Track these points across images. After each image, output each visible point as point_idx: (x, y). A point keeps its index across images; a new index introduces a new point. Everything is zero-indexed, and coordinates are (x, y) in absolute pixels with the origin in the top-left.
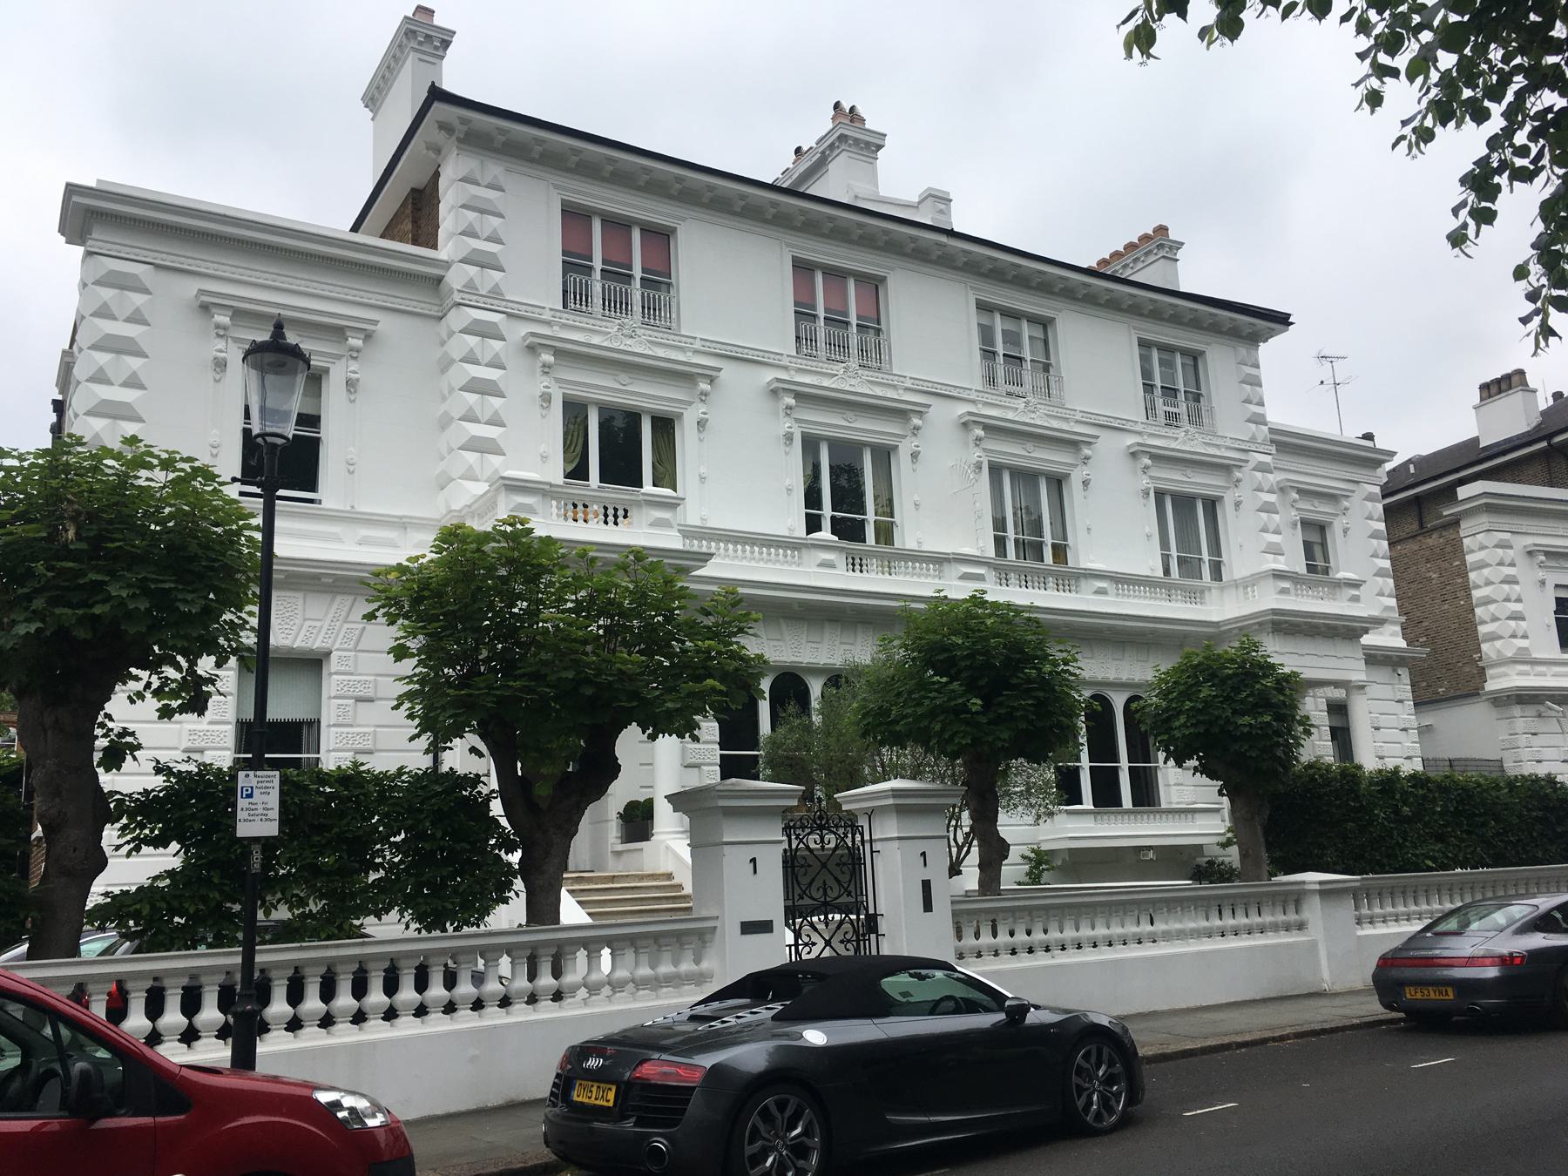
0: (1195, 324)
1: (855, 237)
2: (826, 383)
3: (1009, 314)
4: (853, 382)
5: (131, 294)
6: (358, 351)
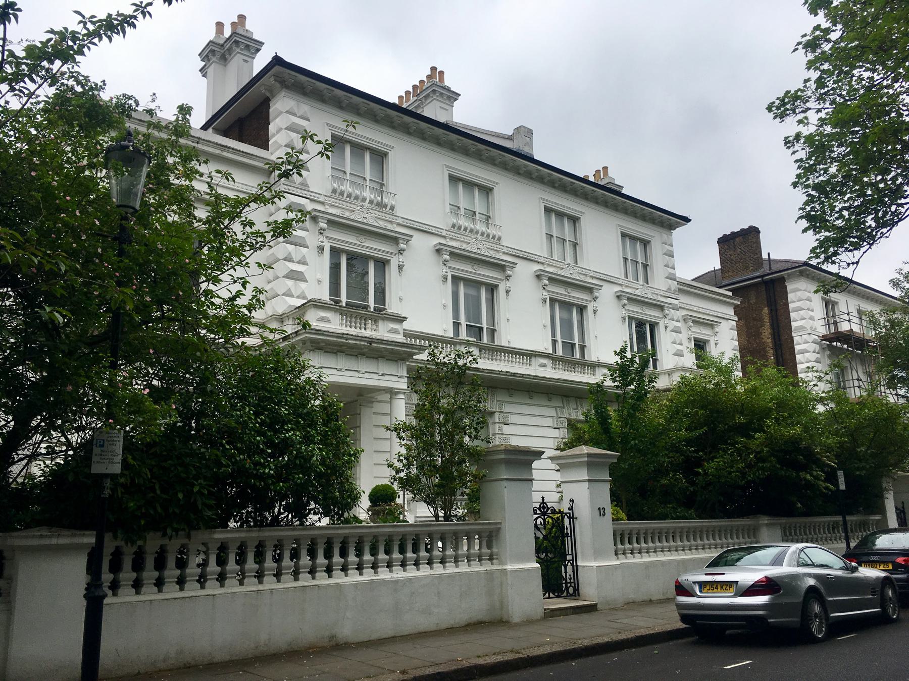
2: (464, 246)
3: (469, 185)
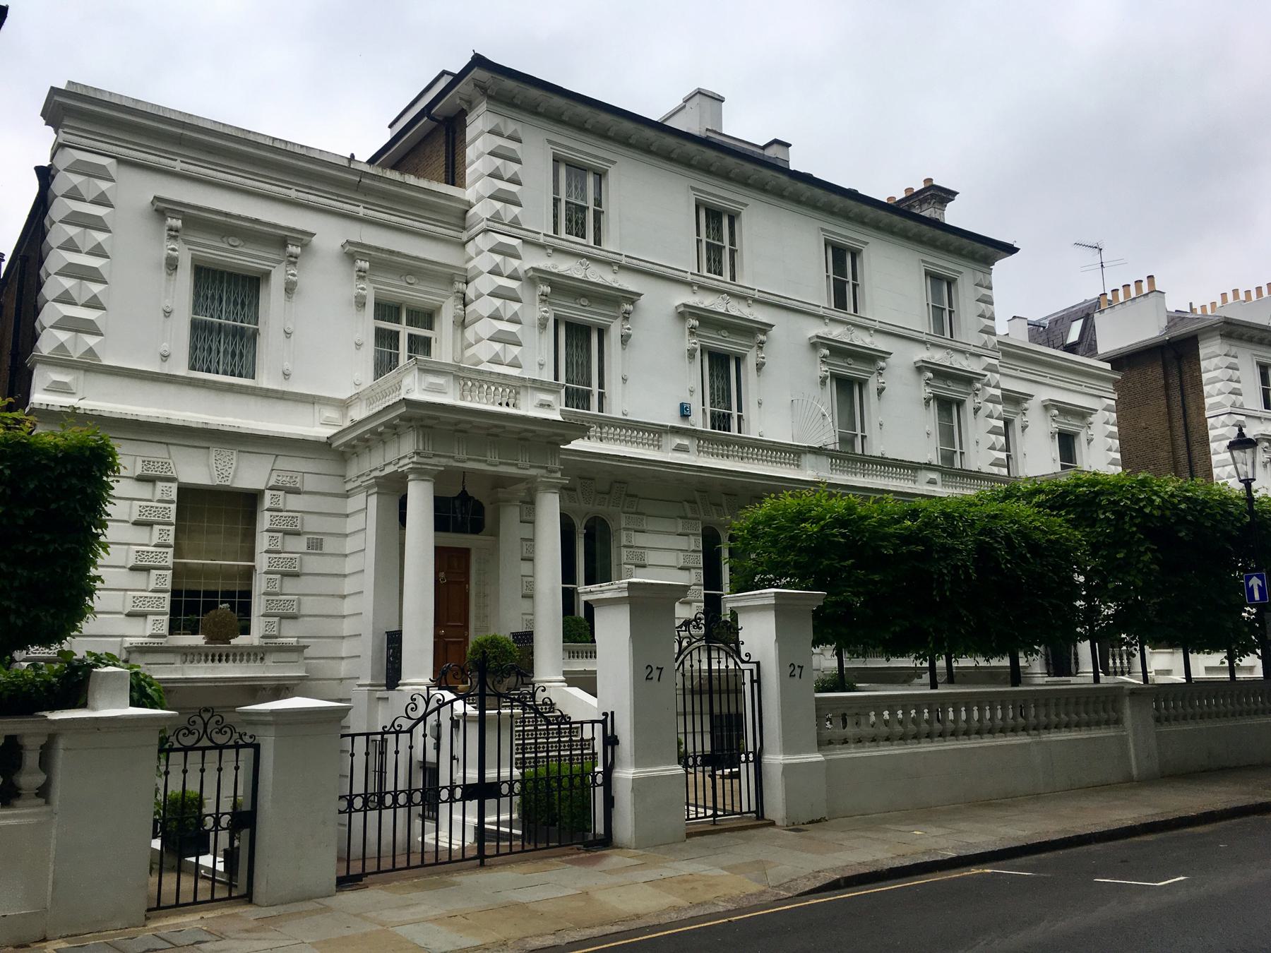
0: (744, 182)
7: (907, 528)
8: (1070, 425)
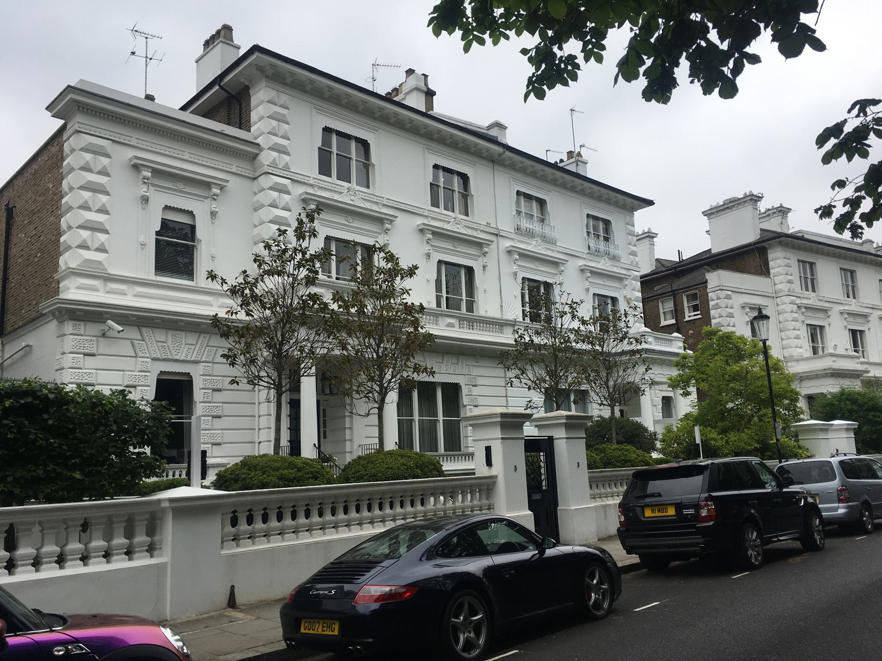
0: (856, 260)
1: (539, 176)
4: (352, 198)
5: (100, 157)
6: (148, 179)
7: (240, 321)
8: (541, 274)
